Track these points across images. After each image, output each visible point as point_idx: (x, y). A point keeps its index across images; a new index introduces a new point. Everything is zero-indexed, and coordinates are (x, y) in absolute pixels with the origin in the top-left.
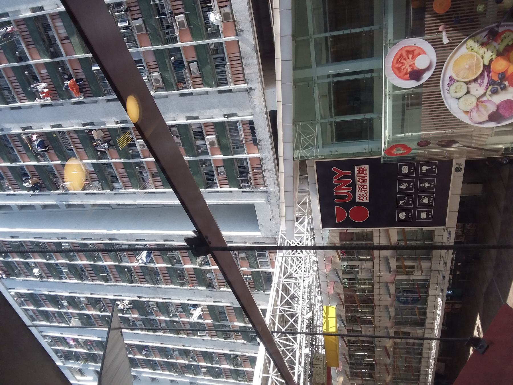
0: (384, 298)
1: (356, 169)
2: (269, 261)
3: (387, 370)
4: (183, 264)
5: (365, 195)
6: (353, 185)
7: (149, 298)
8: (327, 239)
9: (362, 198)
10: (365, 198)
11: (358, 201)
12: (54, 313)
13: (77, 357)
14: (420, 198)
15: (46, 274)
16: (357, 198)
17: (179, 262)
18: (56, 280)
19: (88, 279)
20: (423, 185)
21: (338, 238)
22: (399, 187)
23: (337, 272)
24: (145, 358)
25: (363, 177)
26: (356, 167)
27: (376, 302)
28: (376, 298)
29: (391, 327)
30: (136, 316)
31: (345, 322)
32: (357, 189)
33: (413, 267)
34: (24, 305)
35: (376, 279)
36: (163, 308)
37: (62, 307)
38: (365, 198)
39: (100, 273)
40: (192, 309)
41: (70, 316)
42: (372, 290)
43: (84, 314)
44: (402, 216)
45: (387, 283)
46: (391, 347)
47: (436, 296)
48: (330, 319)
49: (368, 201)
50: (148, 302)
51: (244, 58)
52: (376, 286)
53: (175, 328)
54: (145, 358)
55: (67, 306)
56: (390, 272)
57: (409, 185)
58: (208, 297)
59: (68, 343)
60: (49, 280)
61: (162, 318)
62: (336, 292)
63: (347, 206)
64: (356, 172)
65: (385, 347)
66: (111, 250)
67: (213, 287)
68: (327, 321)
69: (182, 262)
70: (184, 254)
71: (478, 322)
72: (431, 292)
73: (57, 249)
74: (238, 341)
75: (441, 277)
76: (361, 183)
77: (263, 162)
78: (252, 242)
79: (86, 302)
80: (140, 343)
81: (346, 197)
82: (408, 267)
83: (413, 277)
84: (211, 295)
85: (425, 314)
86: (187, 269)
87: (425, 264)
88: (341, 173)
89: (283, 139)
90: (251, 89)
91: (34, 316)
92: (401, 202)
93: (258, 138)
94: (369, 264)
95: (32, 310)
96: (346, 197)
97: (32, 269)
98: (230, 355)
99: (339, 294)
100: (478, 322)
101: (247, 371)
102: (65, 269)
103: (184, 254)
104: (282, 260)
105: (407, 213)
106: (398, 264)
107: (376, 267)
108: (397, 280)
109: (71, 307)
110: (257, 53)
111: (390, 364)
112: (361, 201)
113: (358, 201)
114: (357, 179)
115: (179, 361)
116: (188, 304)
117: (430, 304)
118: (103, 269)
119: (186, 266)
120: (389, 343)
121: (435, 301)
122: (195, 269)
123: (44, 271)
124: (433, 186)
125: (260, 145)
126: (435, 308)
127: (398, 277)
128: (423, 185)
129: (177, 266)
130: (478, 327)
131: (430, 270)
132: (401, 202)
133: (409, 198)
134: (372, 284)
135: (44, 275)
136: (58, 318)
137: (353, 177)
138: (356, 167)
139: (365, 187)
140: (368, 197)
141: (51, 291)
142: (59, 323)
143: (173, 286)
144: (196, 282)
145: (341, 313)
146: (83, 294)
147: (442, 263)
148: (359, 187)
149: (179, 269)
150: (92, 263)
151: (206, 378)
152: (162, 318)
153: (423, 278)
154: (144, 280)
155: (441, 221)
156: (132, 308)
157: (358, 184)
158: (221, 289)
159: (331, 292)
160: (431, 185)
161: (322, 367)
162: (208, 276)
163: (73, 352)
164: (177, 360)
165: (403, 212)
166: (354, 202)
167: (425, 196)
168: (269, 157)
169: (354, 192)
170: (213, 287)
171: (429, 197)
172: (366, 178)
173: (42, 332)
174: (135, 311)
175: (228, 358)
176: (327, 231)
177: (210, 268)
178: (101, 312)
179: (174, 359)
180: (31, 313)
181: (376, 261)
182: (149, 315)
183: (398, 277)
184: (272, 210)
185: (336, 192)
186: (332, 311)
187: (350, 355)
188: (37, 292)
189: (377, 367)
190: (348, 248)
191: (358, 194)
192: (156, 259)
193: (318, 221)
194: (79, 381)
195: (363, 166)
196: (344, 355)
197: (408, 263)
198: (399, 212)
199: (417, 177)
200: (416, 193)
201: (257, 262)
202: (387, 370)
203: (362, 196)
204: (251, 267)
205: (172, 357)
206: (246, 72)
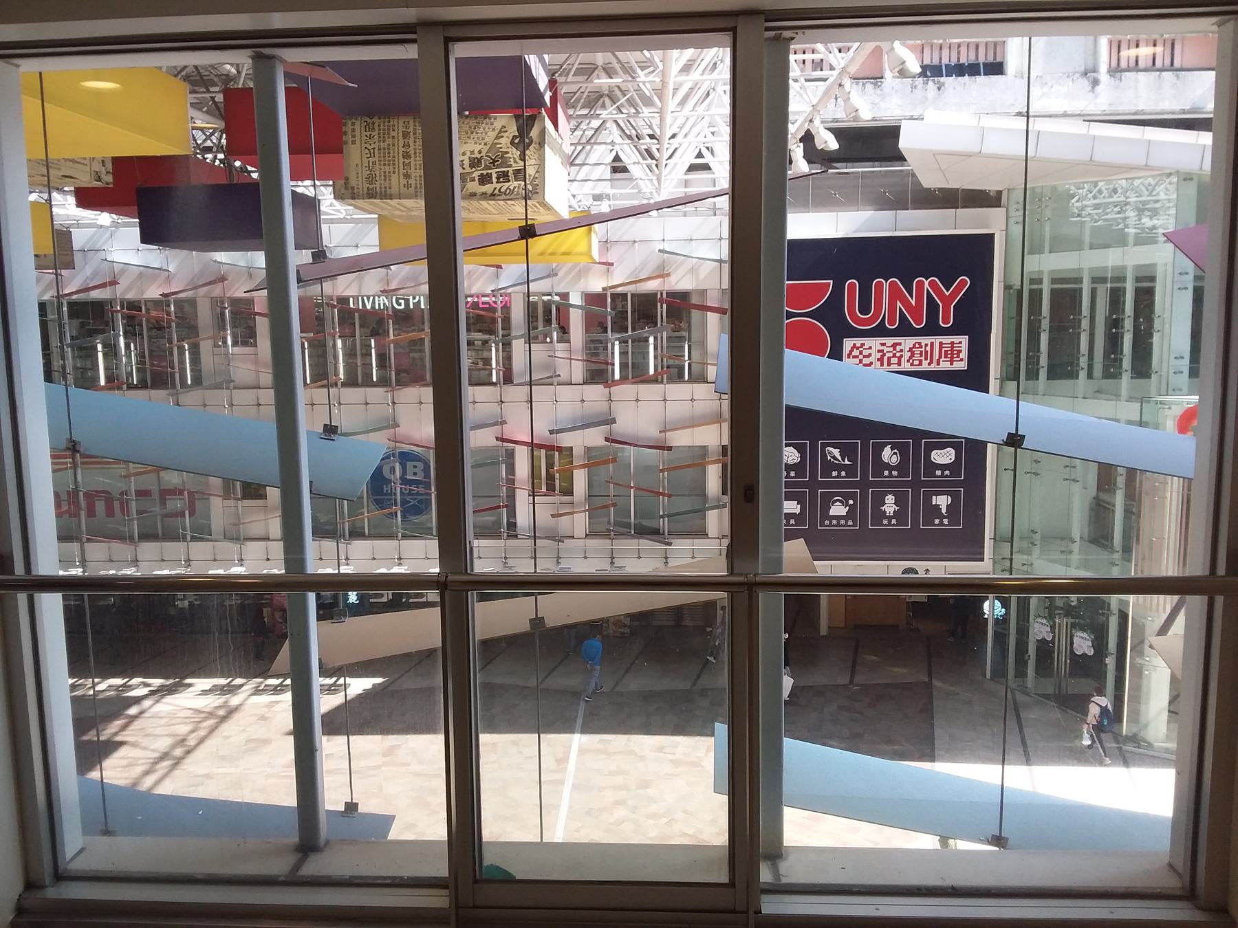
1: (956, 339)
6: (905, 330)
9: (856, 352)
14: (846, 497)
16: (858, 341)
20: (890, 499)
22: (886, 444)
25: (929, 355)
26: (964, 340)
32: (890, 341)
51: (1178, 77)
56: (551, 432)
62: (122, 272)
64: (947, 340)
76: (910, 350)
77: (869, 87)
81: (865, 310)
87: (581, 522)
88: (947, 301)
90: (1095, 82)
92: (836, 452)
93: (950, 82)
96: (865, 310)
99: (114, 283)
107: (565, 392)
108: (511, 455)
110: (1184, 112)
114: (925, 340)
124: (885, 522)
125: (926, 83)
128: (890, 499)
132: (836, 452)
133: (851, 470)
137: (932, 329)
138: (964, 340)
139: (894, 360)
148: (894, 346)
157: (907, 342)
160: (890, 518)
167: (852, 509)
168: (882, 105)
169: (880, 331)
171: (850, 515)
172: (925, 363)
185: (885, 286)
195: (964, 355)
197: (580, 480)
199: (916, 484)
200: (864, 485)
203: (866, 352)
206: (1142, 76)
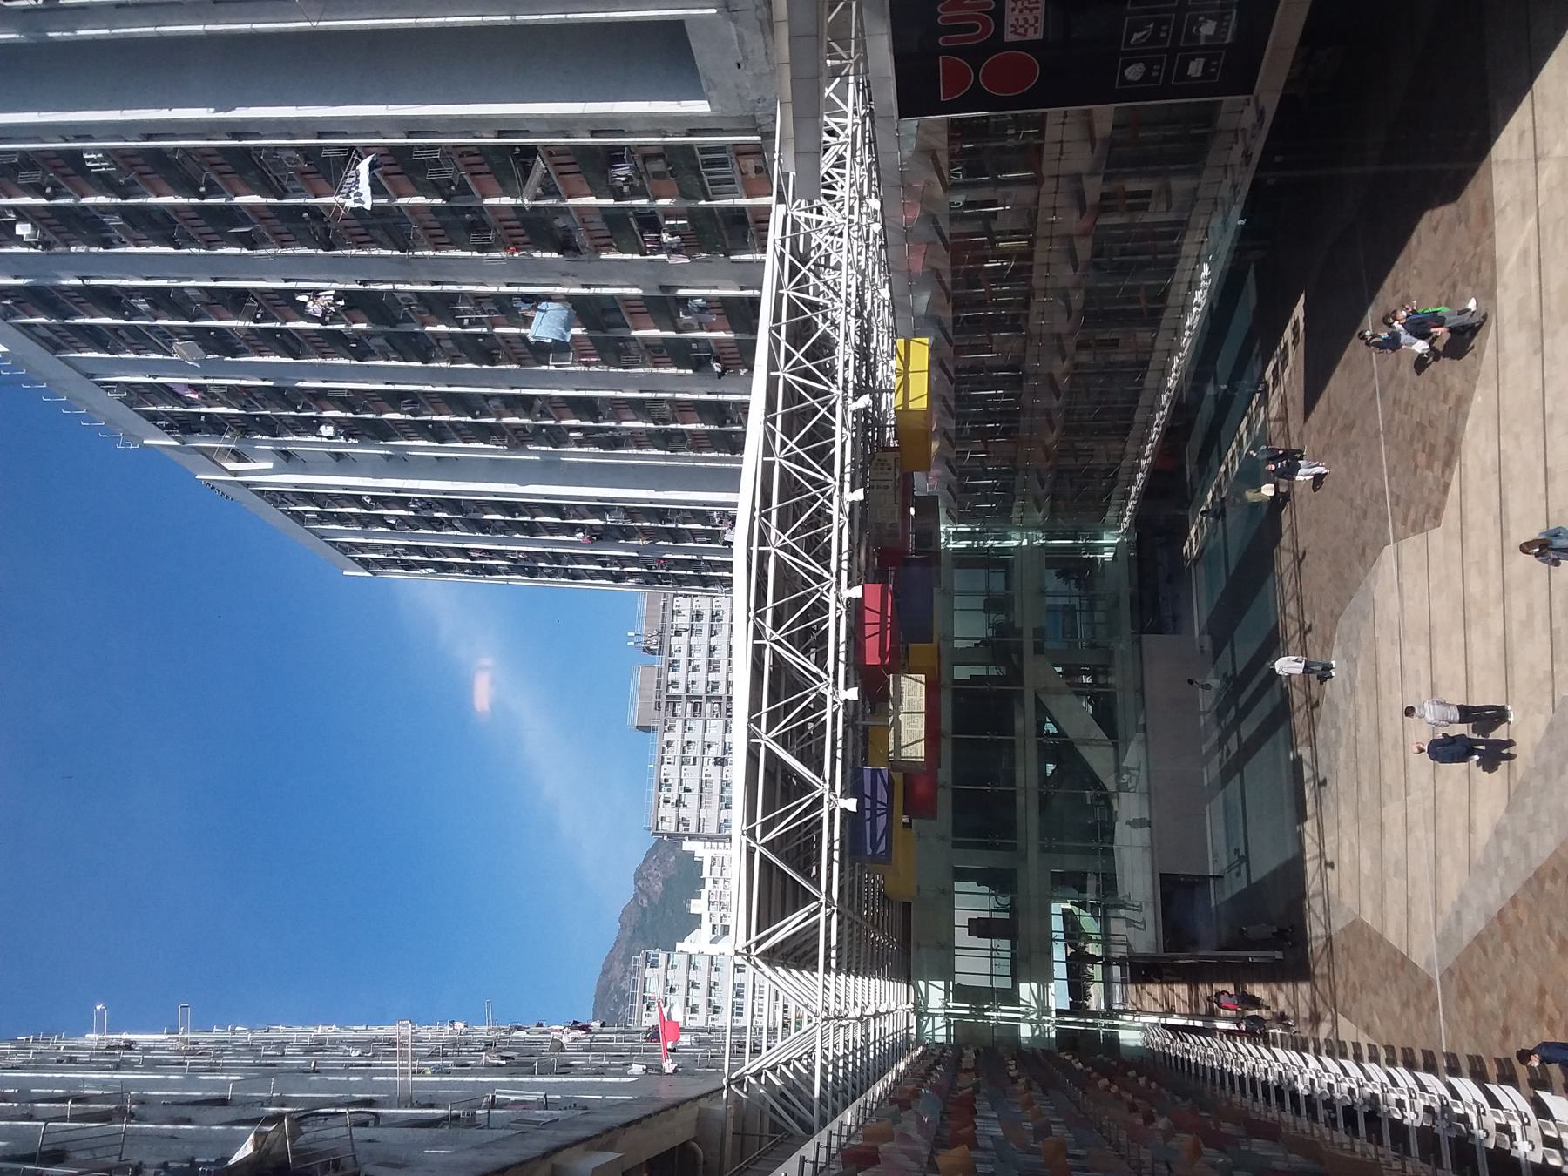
0: (1057, 273)
2: (738, 177)
3: (1050, 422)
4: (478, 195)
5: (1032, 21)
7: (393, 282)
8: (913, 141)
9: (1021, 31)
10: (1031, 30)
11: (1010, 37)
12: (114, 329)
13: (216, 426)
15: (57, 234)
16: (1008, 29)
17: (464, 190)
18: (94, 250)
19: (192, 242)
21: (945, 137)
23: (935, 221)
24: (409, 417)
27: (1037, 282)
28: (1050, 150)
29: (1072, 334)
30: (363, 326)
31: (950, 333)
33: (1148, 194)
34: (14, 315)
35: (1042, 230)
36: (442, 305)
37: (135, 313)
38: (1031, 30)
39: (222, 223)
40: (524, 307)
41: (169, 335)
42: (1027, 255)
43: (209, 329)
44: (1134, 72)
45: (1069, 238)
46: (1065, 374)
47: (1199, 260)
48: (910, 378)
49: (1039, 36)
50: (390, 293)
52: (1041, 246)
53: (485, 351)
54: (409, 417)
55: (147, 311)
57: (1157, 31)
58: (565, 275)
59: (179, 396)
60: (73, 249)
61: (442, 328)
63: (974, 55)
65: (1051, 376)
66: (247, 165)
67: (577, 250)
68: (906, 383)
69: (474, 189)
70: (476, 169)
71: (1299, 311)
72: (1188, 248)
73: (68, 168)
74: (661, 370)
75: (1238, 150)
78: (685, 129)
79: (207, 300)
80: (390, 387)
82: (1135, 195)
83: (1147, 218)
84: (572, 271)
85: (1163, 298)
86: (492, 208)
87: (1179, 185)
89: (790, 20)
91: (55, 338)
92: (1136, 36)
94: (1027, 194)
95: (44, 325)
97: (12, 225)
98: (642, 400)
99: (937, 274)
100: (1299, 311)
101: (690, 431)
102: (114, 221)
103: (476, 169)
104: (783, 244)
105: (1149, 66)
106: (1106, 189)
107: (1046, 201)
109: (162, 312)
111: (1059, 409)
112: (1018, 38)
113: (1010, 37)
115: (506, 420)
116: (511, 295)
117: (1182, 275)
118: (232, 215)
119: (487, 201)
120: (1060, 368)
121: (1196, 272)
122: (518, 209)
123: (48, 226)
126: (1193, 285)
127: (1102, 221)
129: (460, 202)
130: (1297, 322)
131: (1193, 197)
134: (1032, 243)
135: (50, 237)
136: (131, 341)
140: (1040, 25)
141: (88, 278)
142: (137, 352)
143: (459, 253)
144: (526, 239)
145: (940, 313)
146: (190, 279)
147: (1228, 182)
149: (469, 210)
150: (195, 201)
151: (585, 450)
152: (442, 328)
153: (1171, 217)
154: (368, 238)
155: (1244, 82)
156: (345, 309)
158: (604, 256)
159: (918, 268)
161: (890, 484)
162: (559, 222)
163: (200, 414)
164: (500, 417)
165: (1138, 61)
166: (997, 43)
170: (577, 250)
173: (93, 376)
174: (356, 313)
175: (639, 408)
176: (913, 122)
177: (562, 204)
178: (257, 321)
179: (490, 416)
180: (46, 333)
181: (1049, 185)
182: (400, 322)
183: (1102, 221)
184: (740, 37)
186: (920, 353)
187: (958, 399)
188: (47, 283)
189: (1024, 421)
190: (972, 157)
191: (1010, 19)
192: (391, 183)
193: (889, 95)
194: (236, 473)
196: (944, 400)
197: (1132, 185)
198: (1126, 65)
201: (702, 183)
202: (1050, 422)
203: (1021, 22)
204: (686, 195)
205: (485, 414)
